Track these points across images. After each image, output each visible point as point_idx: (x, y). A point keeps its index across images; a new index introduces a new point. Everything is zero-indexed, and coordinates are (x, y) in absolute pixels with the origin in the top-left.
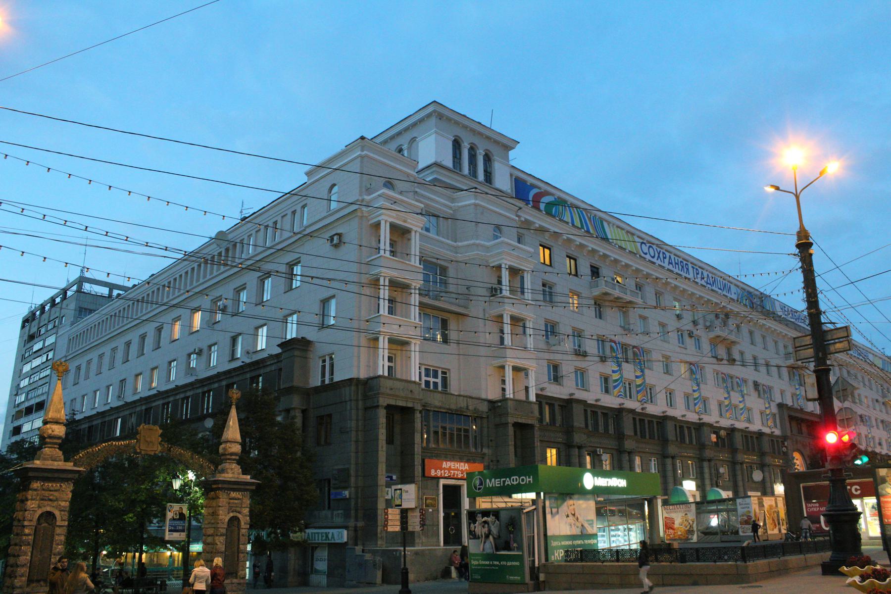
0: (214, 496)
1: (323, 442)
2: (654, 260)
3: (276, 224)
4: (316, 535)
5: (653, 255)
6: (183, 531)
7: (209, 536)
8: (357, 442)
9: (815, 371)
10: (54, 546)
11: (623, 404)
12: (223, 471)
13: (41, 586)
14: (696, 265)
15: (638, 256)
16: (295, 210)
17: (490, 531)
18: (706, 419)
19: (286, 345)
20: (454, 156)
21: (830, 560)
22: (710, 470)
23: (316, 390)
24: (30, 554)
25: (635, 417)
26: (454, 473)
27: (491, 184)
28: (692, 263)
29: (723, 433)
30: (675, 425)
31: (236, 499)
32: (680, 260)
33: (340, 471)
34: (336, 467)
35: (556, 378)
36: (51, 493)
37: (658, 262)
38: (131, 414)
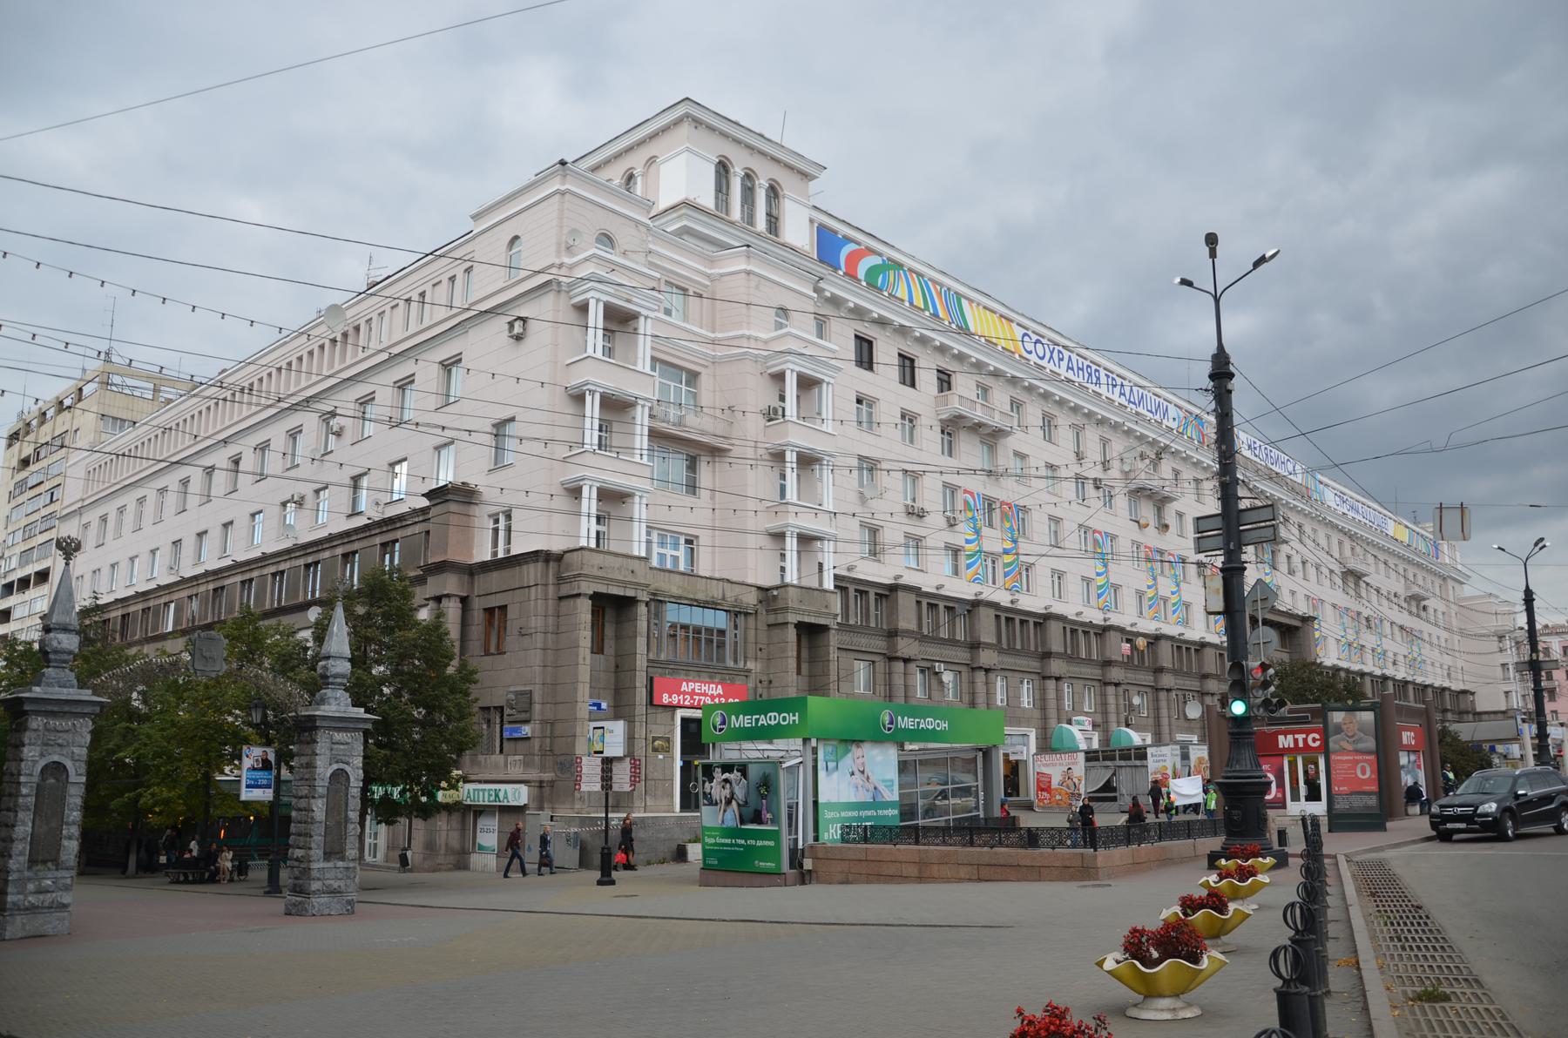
0: (309, 739)
1: (493, 650)
2: (1044, 363)
3: (424, 297)
4: (481, 793)
5: (1041, 355)
6: (268, 787)
7: (301, 797)
9: (1222, 570)
10: (66, 812)
11: (981, 593)
12: (323, 701)
13: (49, 869)
14: (1112, 373)
15: (1017, 356)
16: (455, 276)
17: (732, 794)
18: (1115, 620)
19: (438, 495)
20: (719, 190)
21: (1222, 848)
22: (1117, 700)
23: (485, 567)
24: (30, 825)
25: (998, 613)
26: (700, 700)
27: (777, 236)
28: (1105, 369)
29: (1141, 643)
30: (1064, 628)
31: (343, 744)
32: (1087, 363)
33: (517, 694)
34: (512, 689)
35: (875, 551)
36: (61, 735)
37: (1051, 366)
38: (190, 597)
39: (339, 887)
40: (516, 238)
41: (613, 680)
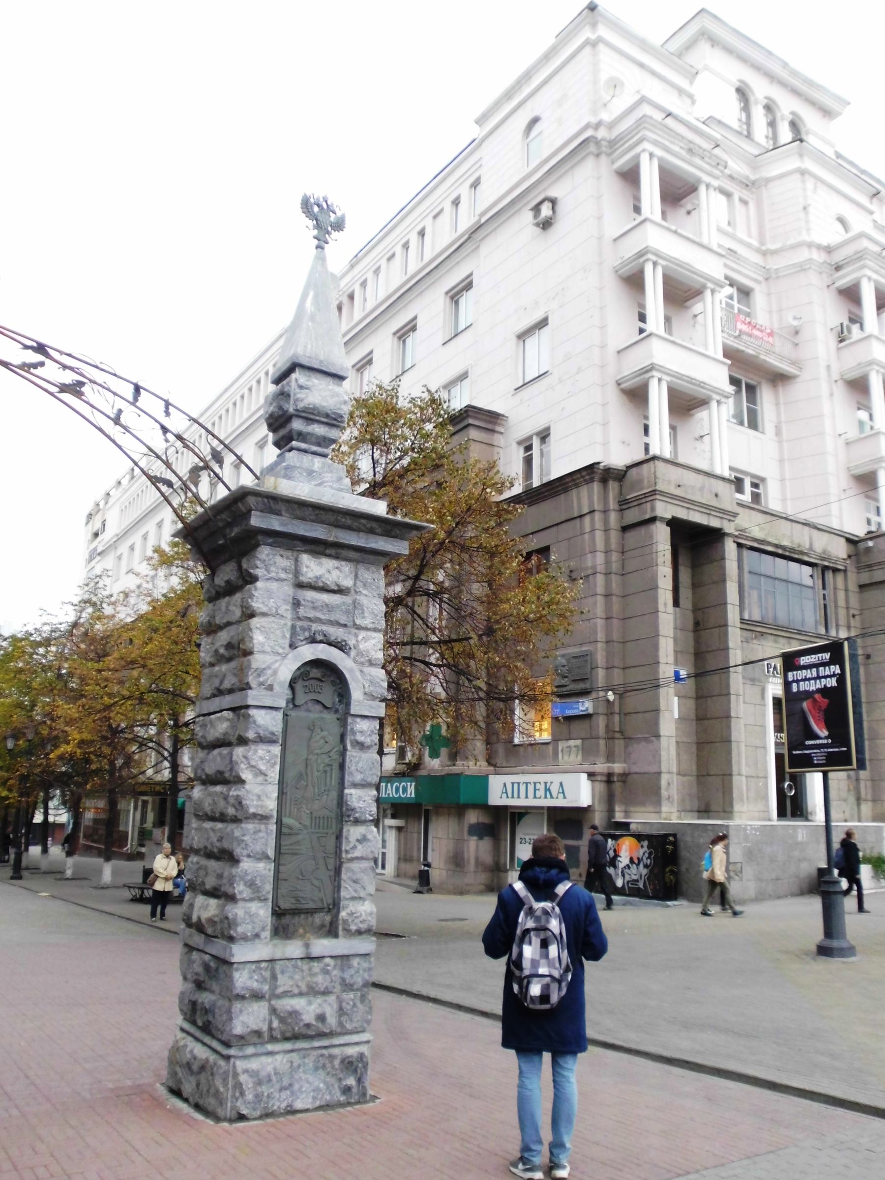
4: (523, 788)
8: (607, 596)
31: (325, 589)
39: (321, 1018)
40: (535, 121)
41: (691, 642)
